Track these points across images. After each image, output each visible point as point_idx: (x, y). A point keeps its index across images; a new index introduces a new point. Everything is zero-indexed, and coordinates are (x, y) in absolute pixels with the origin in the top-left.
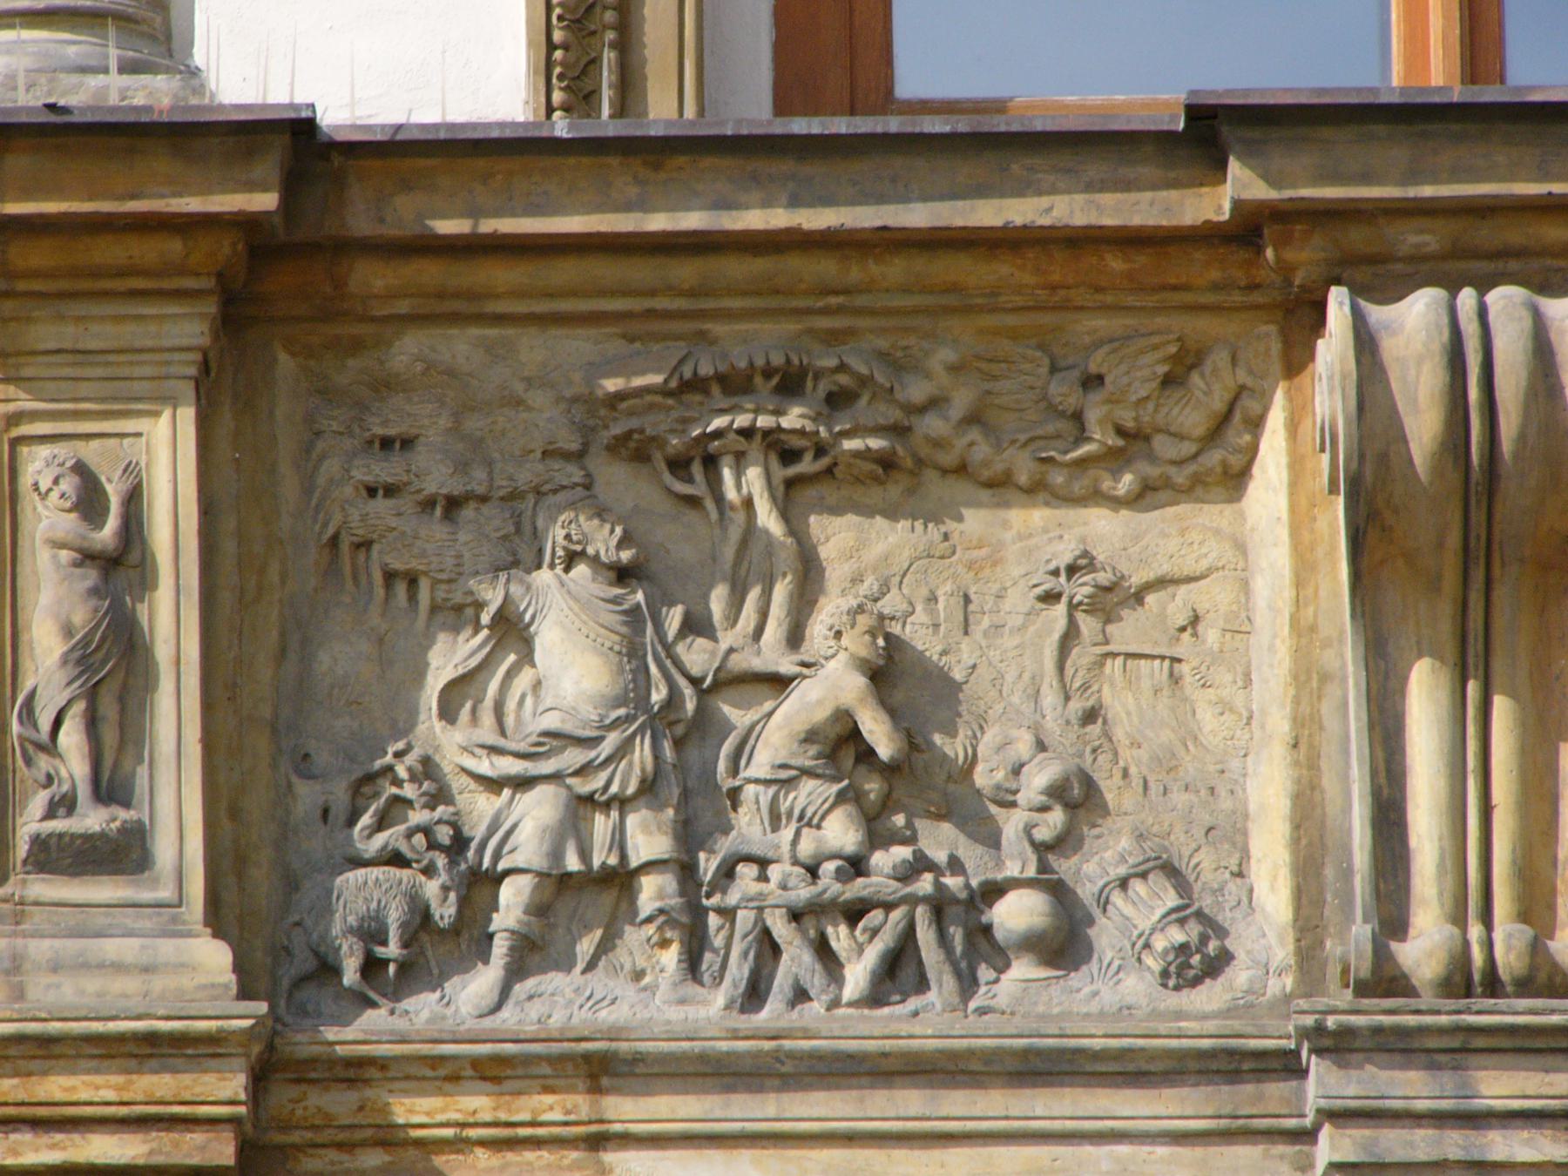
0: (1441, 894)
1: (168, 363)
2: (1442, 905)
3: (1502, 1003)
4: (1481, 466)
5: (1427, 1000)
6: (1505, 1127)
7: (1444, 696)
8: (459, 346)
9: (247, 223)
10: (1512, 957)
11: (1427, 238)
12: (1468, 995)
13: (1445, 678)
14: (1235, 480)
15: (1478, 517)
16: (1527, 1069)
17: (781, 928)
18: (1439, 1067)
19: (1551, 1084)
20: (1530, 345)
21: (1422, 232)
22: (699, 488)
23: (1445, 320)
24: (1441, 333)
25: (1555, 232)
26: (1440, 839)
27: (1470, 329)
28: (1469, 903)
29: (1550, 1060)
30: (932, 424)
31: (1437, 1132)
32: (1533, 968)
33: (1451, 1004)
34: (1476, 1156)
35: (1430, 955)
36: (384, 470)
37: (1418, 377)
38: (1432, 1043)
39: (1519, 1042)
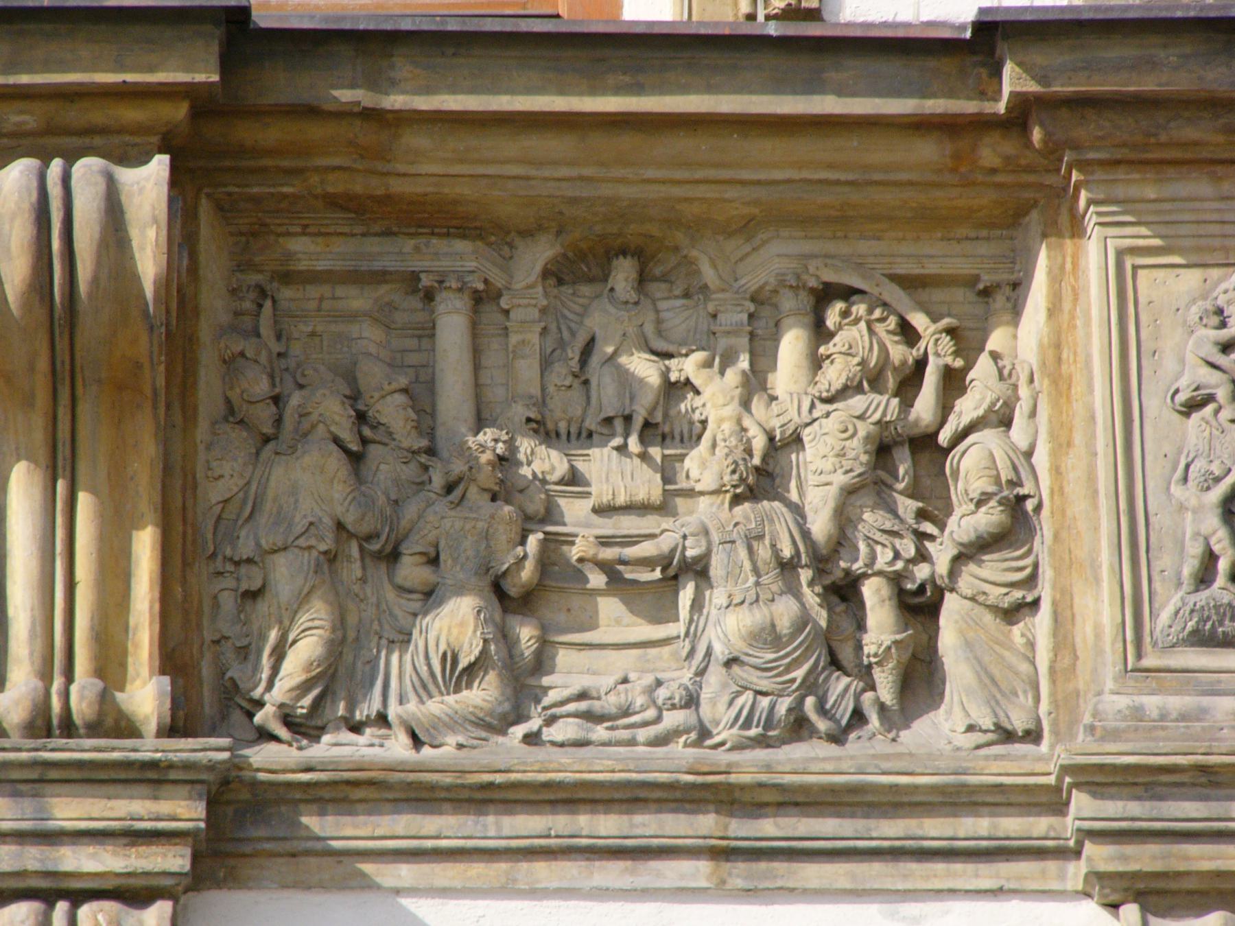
0: (31, 654)
2: (33, 663)
3: (72, 742)
4: (61, 303)
5: (15, 739)
6: (74, 844)
7: (37, 493)
10: (84, 705)
11: (26, 117)
12: (49, 734)
13: (38, 477)
15: (62, 345)
16: (94, 797)
18: (20, 795)
19: (112, 809)
20: (103, 206)
21: (21, 112)
23: (35, 184)
24: (30, 195)
26: (32, 610)
27: (55, 191)
28: (55, 662)
29: (111, 789)
31: (19, 847)
32: (101, 714)
33: (31, 743)
34: (50, 867)
35: (17, 703)
37: (11, 230)
38: (15, 775)
39: (86, 774)
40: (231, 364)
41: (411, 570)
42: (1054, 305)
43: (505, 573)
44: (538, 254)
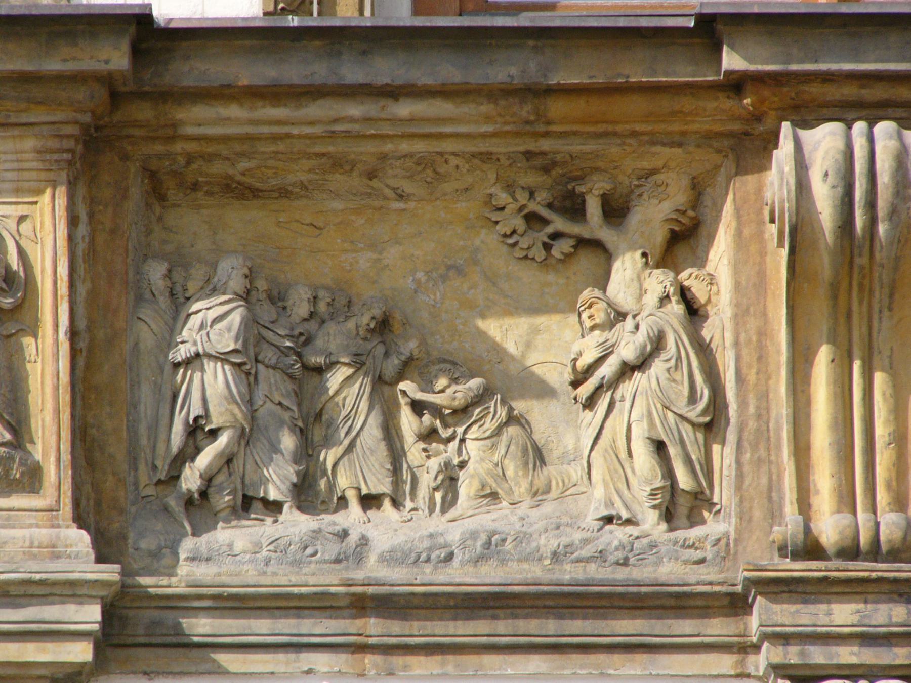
1: (367, 120)
9: (107, 80)
25: (905, 93)
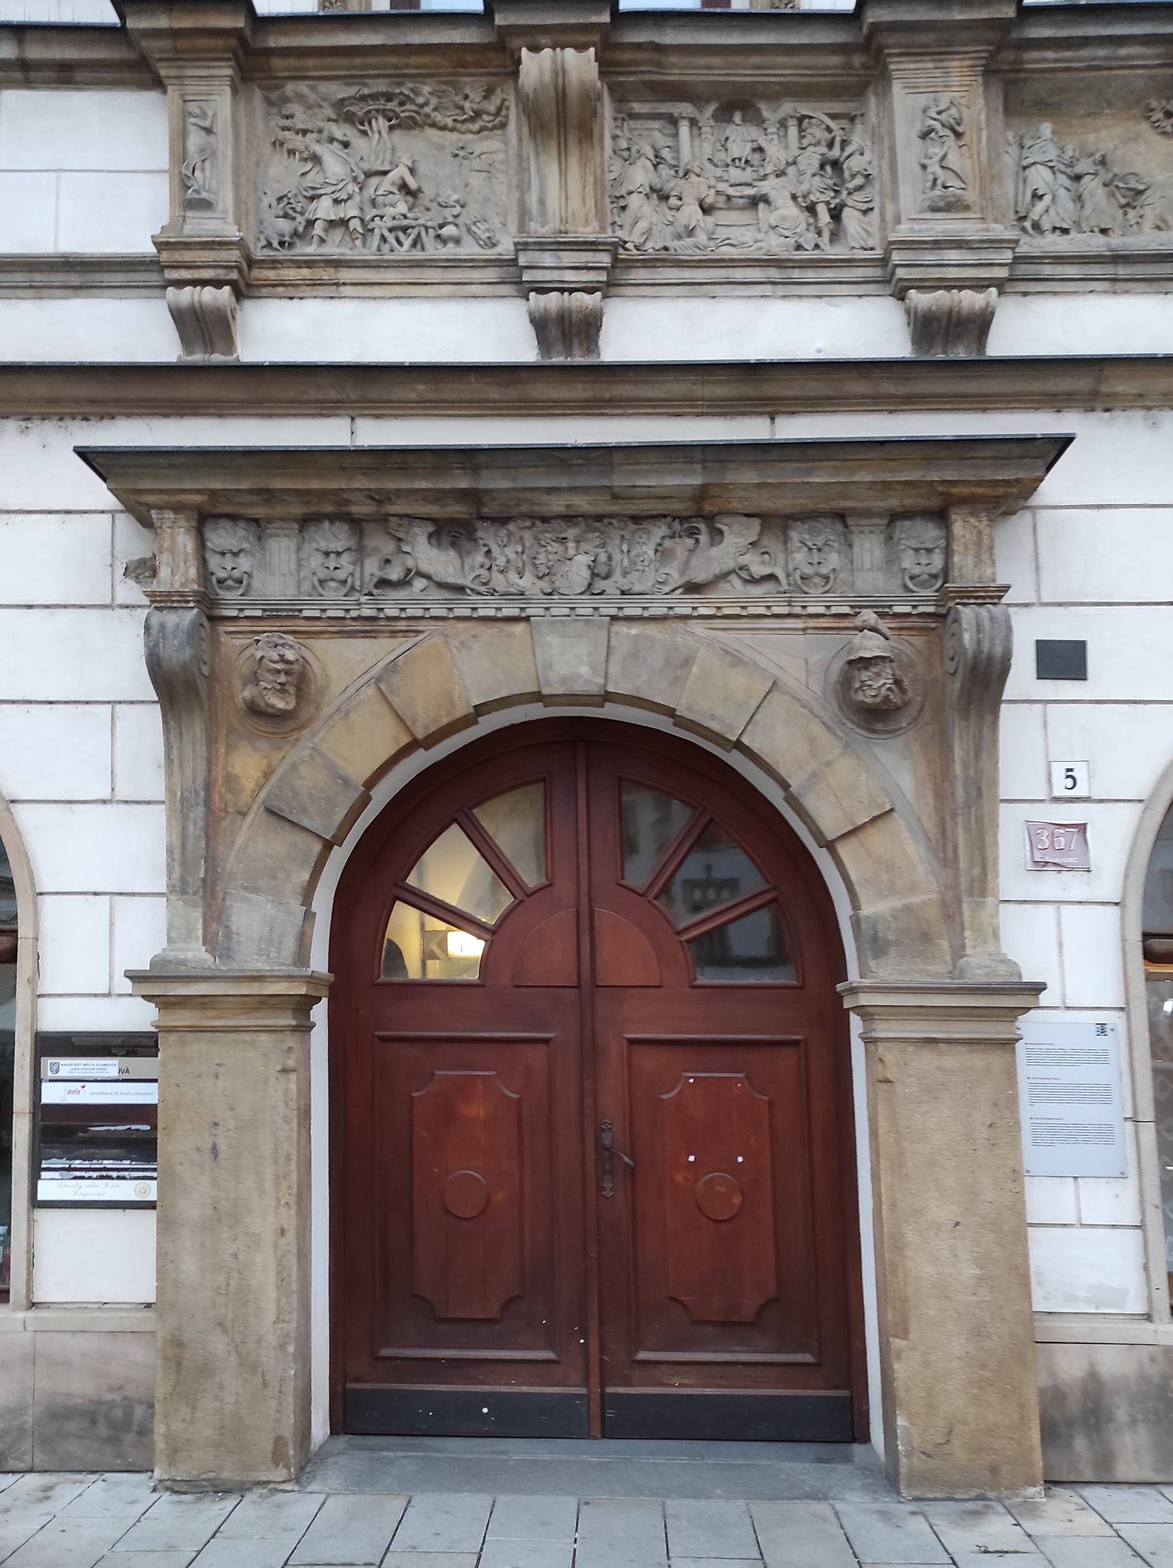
8: (303, 87)
14: (503, 126)
17: (386, 233)
22: (366, 128)
30: (427, 110)
36: (287, 123)
40: (615, 138)
41: (673, 201)
42: (313, 519)
43: (180, 727)
44: (712, 108)
